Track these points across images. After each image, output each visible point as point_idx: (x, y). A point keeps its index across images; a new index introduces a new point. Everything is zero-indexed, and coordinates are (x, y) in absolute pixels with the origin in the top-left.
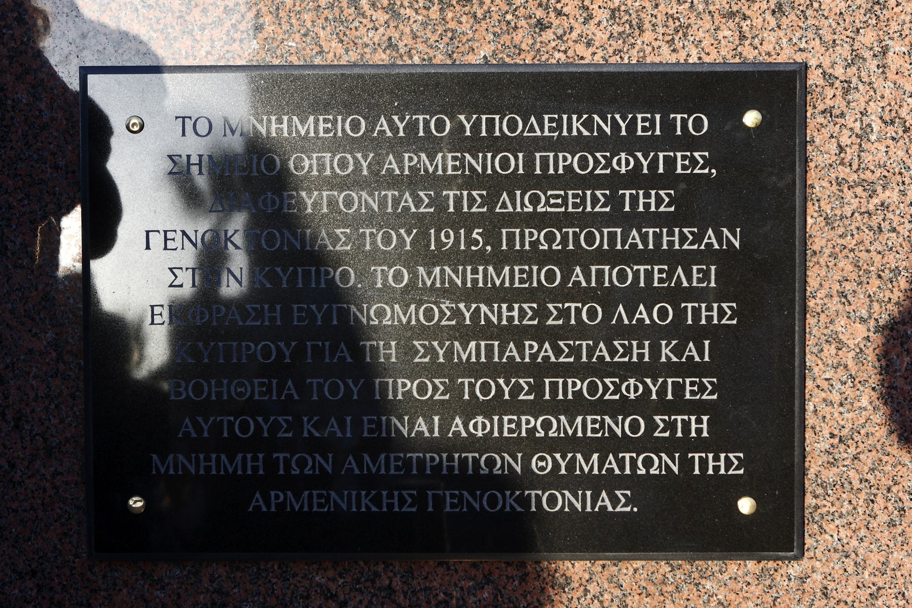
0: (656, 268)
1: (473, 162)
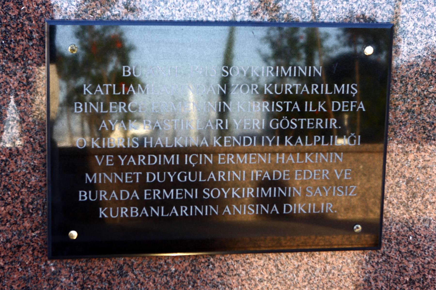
0: (309, 120)
1: (338, 157)
